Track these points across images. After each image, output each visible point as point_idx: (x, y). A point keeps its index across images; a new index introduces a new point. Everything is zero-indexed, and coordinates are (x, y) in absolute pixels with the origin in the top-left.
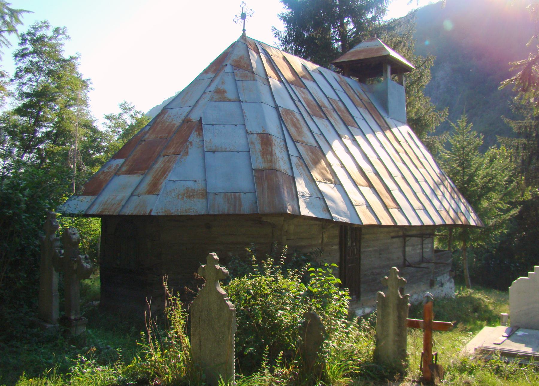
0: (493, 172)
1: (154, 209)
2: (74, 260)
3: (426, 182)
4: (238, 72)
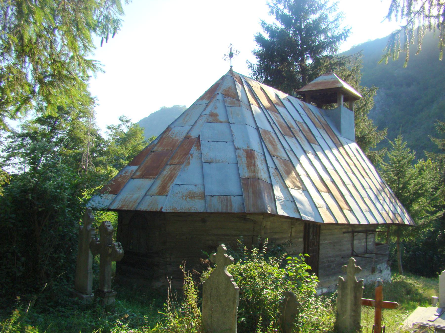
0: (423, 181)
1: (164, 207)
2: (109, 246)
3: (371, 189)
4: (227, 100)
